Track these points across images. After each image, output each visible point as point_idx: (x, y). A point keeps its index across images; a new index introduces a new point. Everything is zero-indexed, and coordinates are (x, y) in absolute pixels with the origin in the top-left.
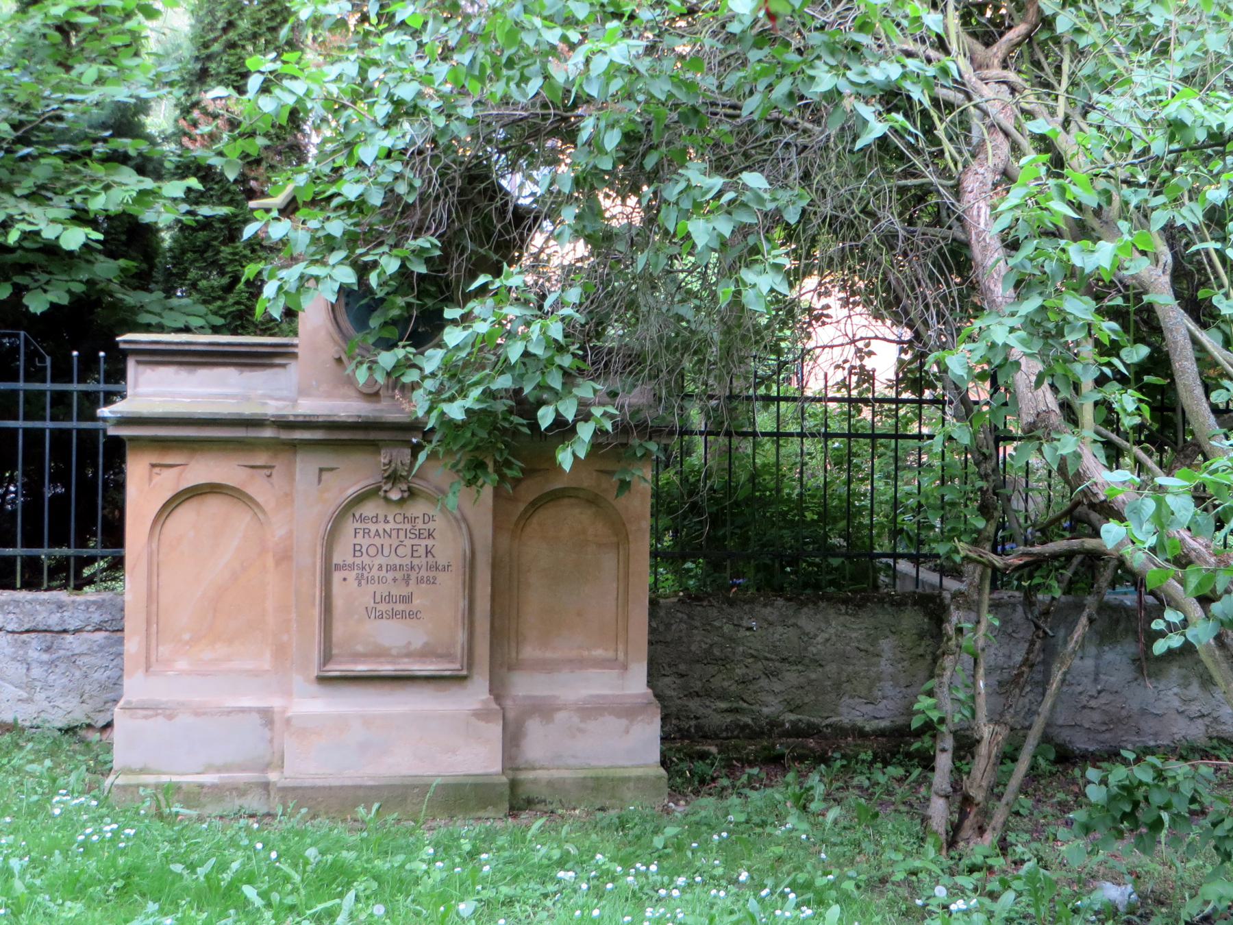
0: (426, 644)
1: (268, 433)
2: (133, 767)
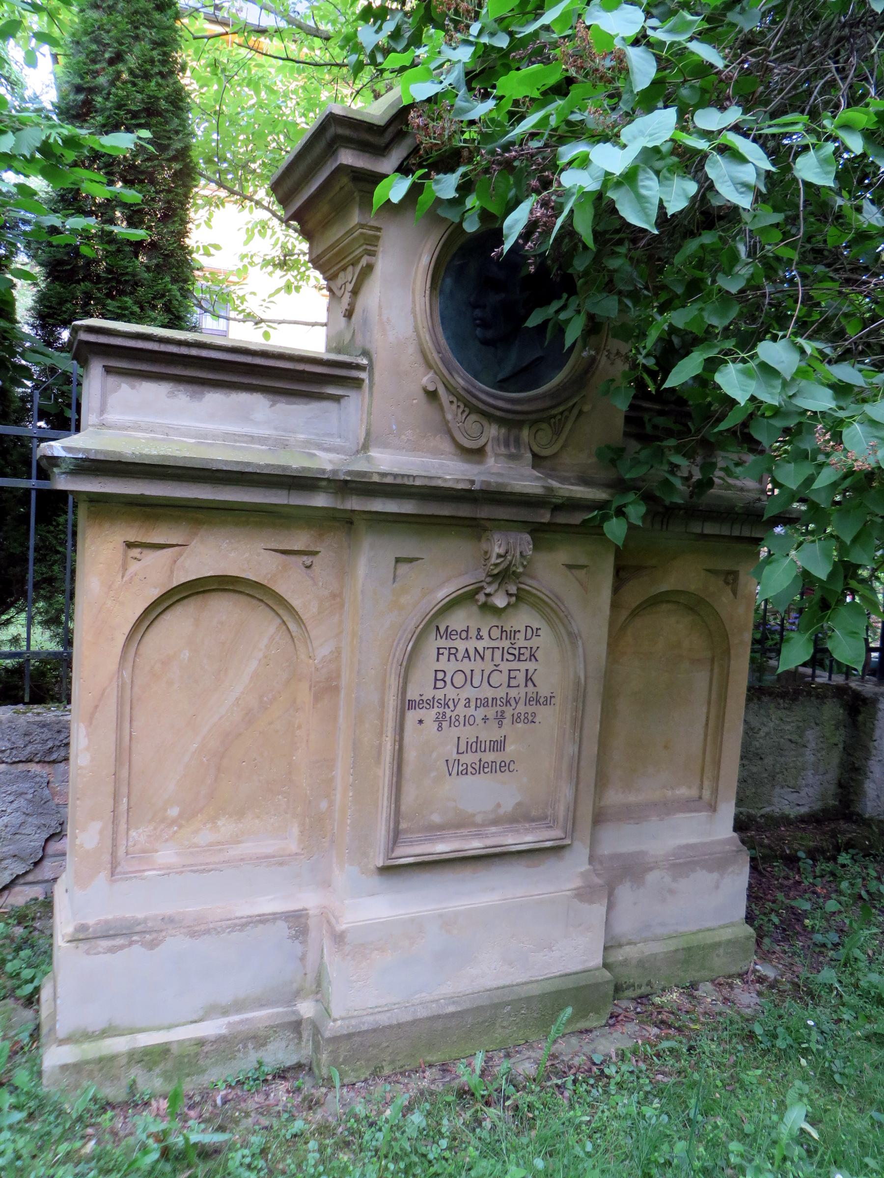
0: (519, 804)
1: (320, 501)
2: (90, 1030)
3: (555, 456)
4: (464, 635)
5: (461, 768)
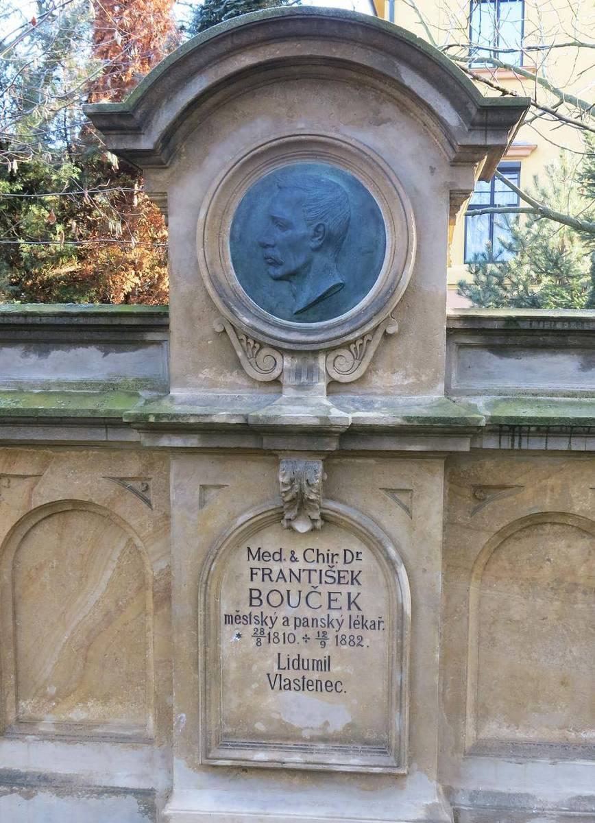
0: (350, 726)
3: (362, 379)
4: (277, 557)
5: (283, 684)
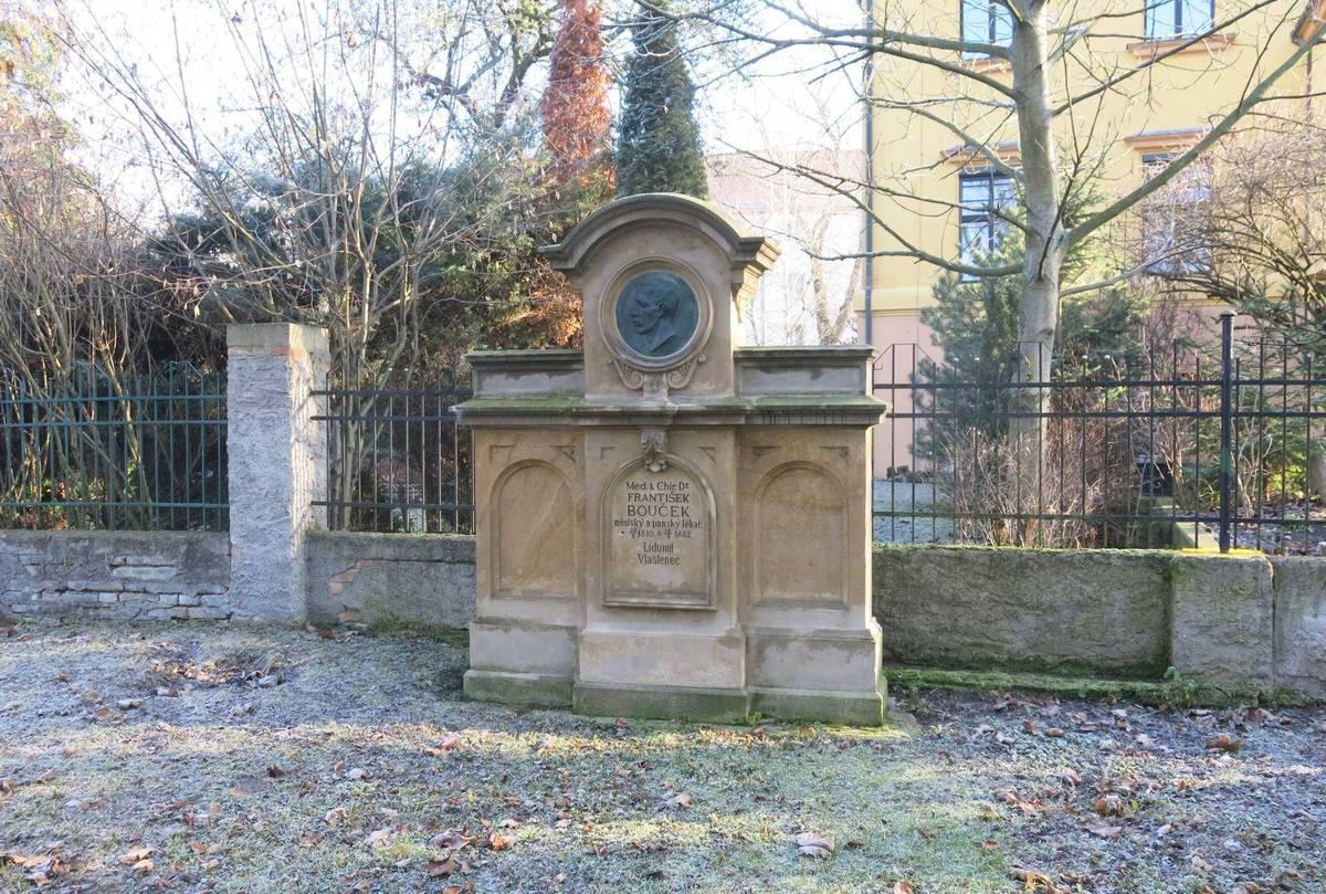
0: (684, 584)
